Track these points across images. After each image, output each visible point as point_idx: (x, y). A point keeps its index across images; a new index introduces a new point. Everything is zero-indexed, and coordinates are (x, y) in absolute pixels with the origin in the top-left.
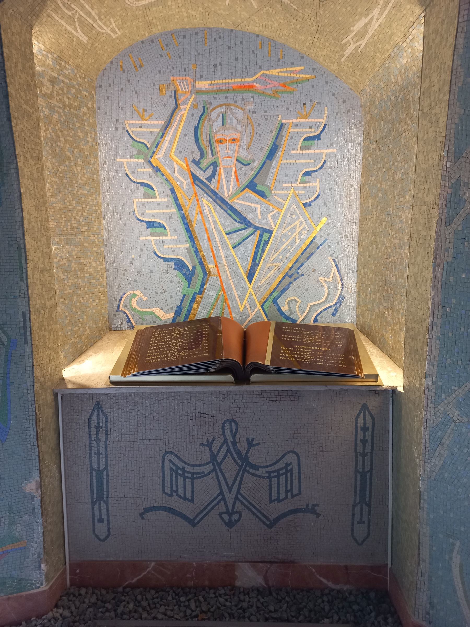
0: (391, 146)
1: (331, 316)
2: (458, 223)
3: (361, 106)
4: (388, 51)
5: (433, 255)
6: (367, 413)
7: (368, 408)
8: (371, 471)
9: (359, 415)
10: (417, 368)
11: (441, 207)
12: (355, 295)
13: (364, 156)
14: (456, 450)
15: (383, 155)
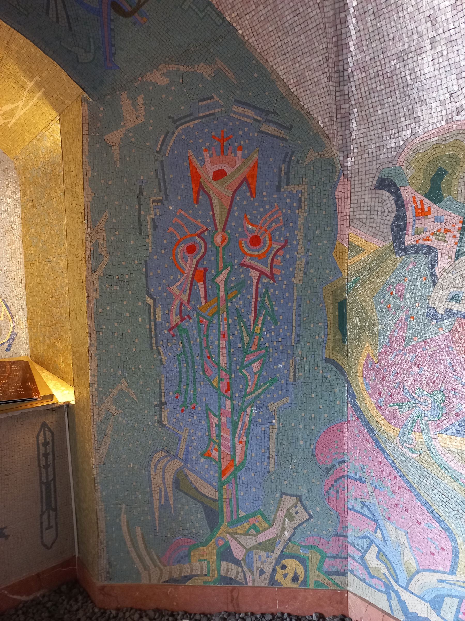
0: (45, 207)
1: (5, 352)
2: (100, 271)
3: (16, 169)
4: (34, 133)
5: (86, 294)
6: (47, 429)
7: (47, 425)
8: (54, 479)
9: (39, 433)
10: (83, 381)
11: (88, 260)
12: (27, 331)
13: (22, 211)
14: (116, 436)
15: (39, 212)
